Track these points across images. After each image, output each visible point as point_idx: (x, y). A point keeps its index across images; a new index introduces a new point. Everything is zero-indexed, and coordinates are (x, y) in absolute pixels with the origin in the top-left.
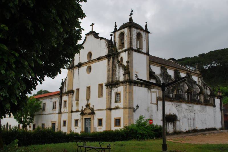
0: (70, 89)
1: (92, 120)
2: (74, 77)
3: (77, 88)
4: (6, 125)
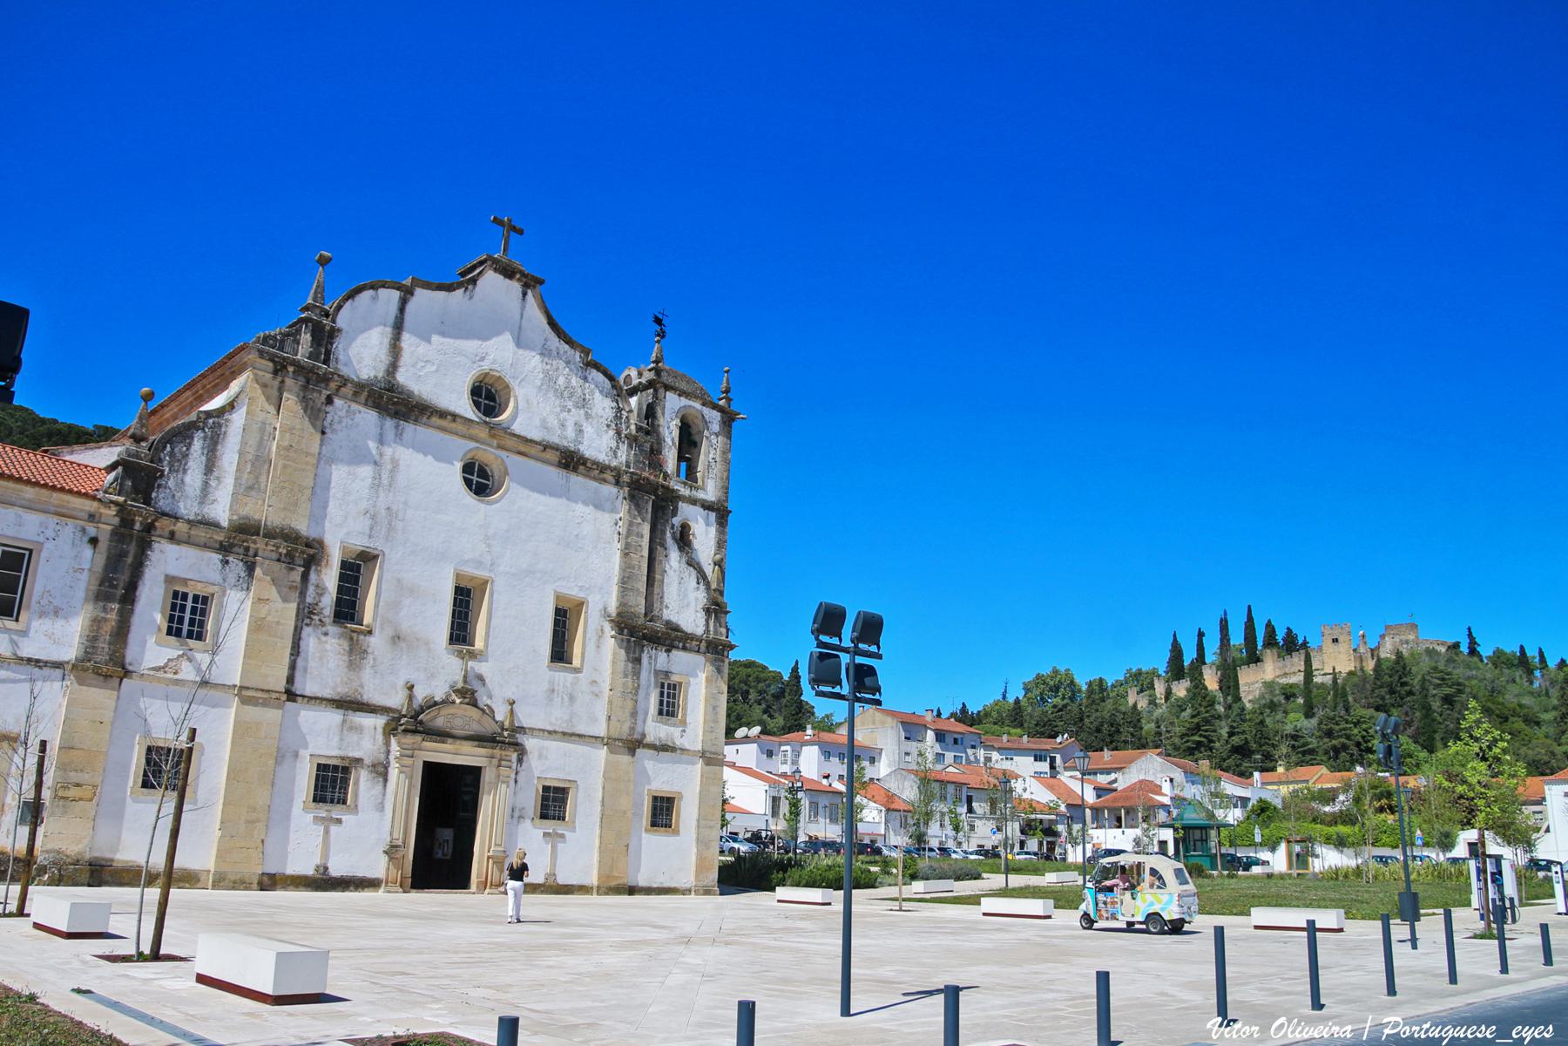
3: (360, 542)
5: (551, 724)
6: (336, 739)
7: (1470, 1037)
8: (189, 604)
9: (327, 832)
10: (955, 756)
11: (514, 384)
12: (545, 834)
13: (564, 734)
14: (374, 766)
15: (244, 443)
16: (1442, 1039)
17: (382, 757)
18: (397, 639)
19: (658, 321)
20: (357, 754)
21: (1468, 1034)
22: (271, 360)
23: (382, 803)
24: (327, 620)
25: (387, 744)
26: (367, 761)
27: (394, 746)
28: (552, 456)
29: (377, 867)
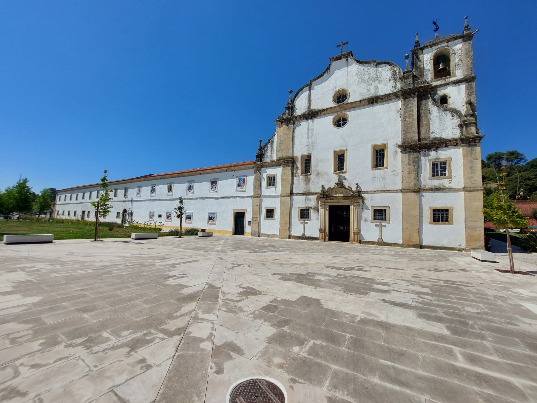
0: (284, 154)
1: (322, 226)
2: (295, 135)
3: (305, 153)
4: (121, 212)
5: (376, 188)
6: (305, 202)
9: (304, 226)
11: (337, 89)
12: (376, 225)
13: (381, 191)
14: (315, 208)
15: (277, 142)
17: (317, 206)
18: (318, 174)
19: (435, 23)
20: (310, 206)
22: (279, 121)
23: (318, 218)
24: (300, 175)
25: (318, 202)
26: (313, 207)
27: (320, 202)
28: (367, 102)
29: (317, 234)
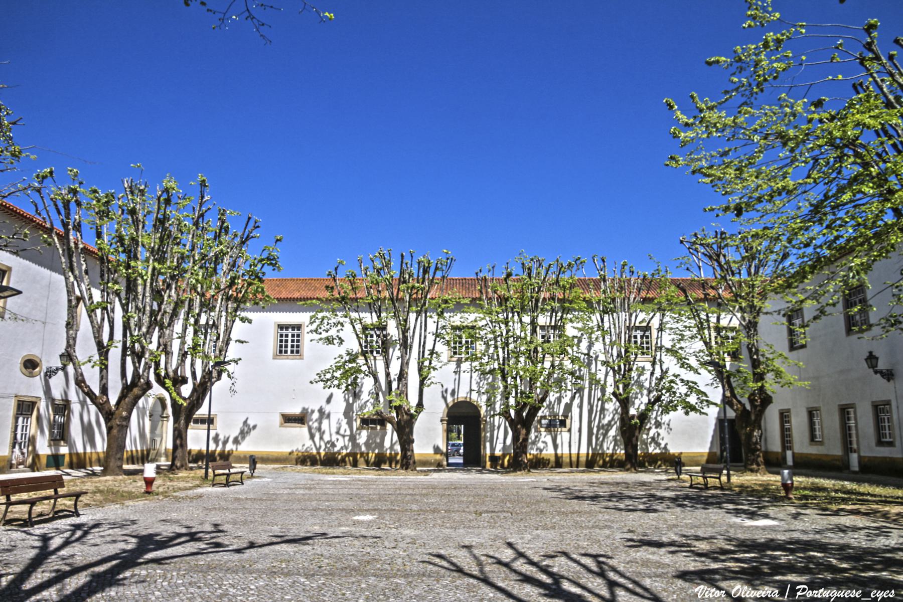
7: (847, 597)
8: (289, 349)
10: (78, 515)
16: (830, 598)
21: (846, 595)
